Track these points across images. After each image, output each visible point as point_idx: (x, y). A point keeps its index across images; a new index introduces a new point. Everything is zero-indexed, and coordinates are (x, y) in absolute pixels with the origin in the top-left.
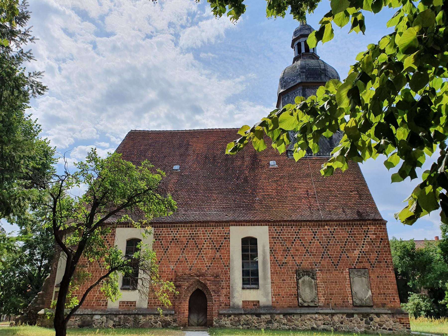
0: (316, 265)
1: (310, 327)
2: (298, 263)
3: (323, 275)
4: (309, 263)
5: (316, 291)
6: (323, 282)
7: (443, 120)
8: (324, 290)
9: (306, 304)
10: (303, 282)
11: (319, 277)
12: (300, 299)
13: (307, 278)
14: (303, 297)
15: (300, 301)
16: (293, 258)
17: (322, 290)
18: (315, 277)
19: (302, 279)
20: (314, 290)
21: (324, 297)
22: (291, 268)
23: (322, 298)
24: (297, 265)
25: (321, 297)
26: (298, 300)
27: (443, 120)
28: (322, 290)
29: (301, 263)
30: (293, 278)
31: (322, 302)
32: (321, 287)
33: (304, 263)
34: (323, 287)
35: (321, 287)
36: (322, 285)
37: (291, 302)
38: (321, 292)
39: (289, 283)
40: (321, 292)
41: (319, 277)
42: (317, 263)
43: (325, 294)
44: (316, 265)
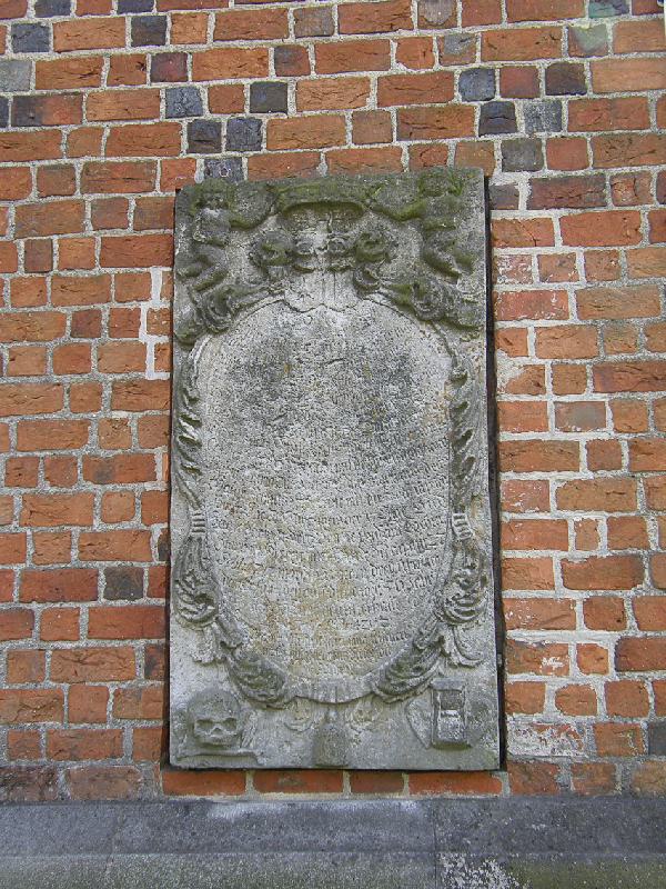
0: (499, 119)
1: (121, 796)
2: (225, 99)
3: (602, 266)
4: (392, 89)
5: (478, 522)
6: (606, 377)
7: (7, 289)
8: (614, 497)
9: (275, 739)
10: (270, 371)
11: (536, 304)
12: (185, 645)
13: (324, 307)
14: (243, 608)
15: (188, 680)
16: (150, 32)
17: (574, 496)
18: (470, 287)
19: (260, 323)
20: (436, 497)
21: (598, 615)
22: (95, 179)
23: (582, 634)
24: (204, 138)
25: (559, 617)
26: (159, 664)
27: (7, 289)
28: (574, 496)
29: (270, 98)
30: (128, 323)
31: (575, 700)
32: (564, 456)
33: (314, 97)
34: (602, 455)
35: (564, 456)
36: (591, 417)
37: (52, 705)
38: (554, 536)
39: (47, 398)
40: (554, 536)
41: (536, 304)
42: (522, 85)
43: (629, 571)
44: (499, 119)
